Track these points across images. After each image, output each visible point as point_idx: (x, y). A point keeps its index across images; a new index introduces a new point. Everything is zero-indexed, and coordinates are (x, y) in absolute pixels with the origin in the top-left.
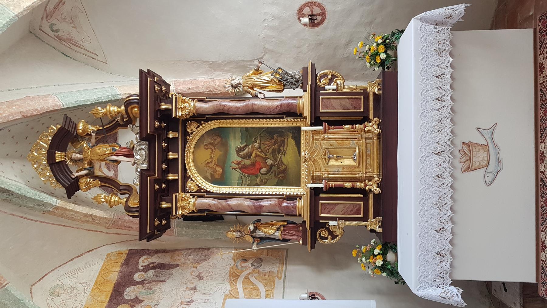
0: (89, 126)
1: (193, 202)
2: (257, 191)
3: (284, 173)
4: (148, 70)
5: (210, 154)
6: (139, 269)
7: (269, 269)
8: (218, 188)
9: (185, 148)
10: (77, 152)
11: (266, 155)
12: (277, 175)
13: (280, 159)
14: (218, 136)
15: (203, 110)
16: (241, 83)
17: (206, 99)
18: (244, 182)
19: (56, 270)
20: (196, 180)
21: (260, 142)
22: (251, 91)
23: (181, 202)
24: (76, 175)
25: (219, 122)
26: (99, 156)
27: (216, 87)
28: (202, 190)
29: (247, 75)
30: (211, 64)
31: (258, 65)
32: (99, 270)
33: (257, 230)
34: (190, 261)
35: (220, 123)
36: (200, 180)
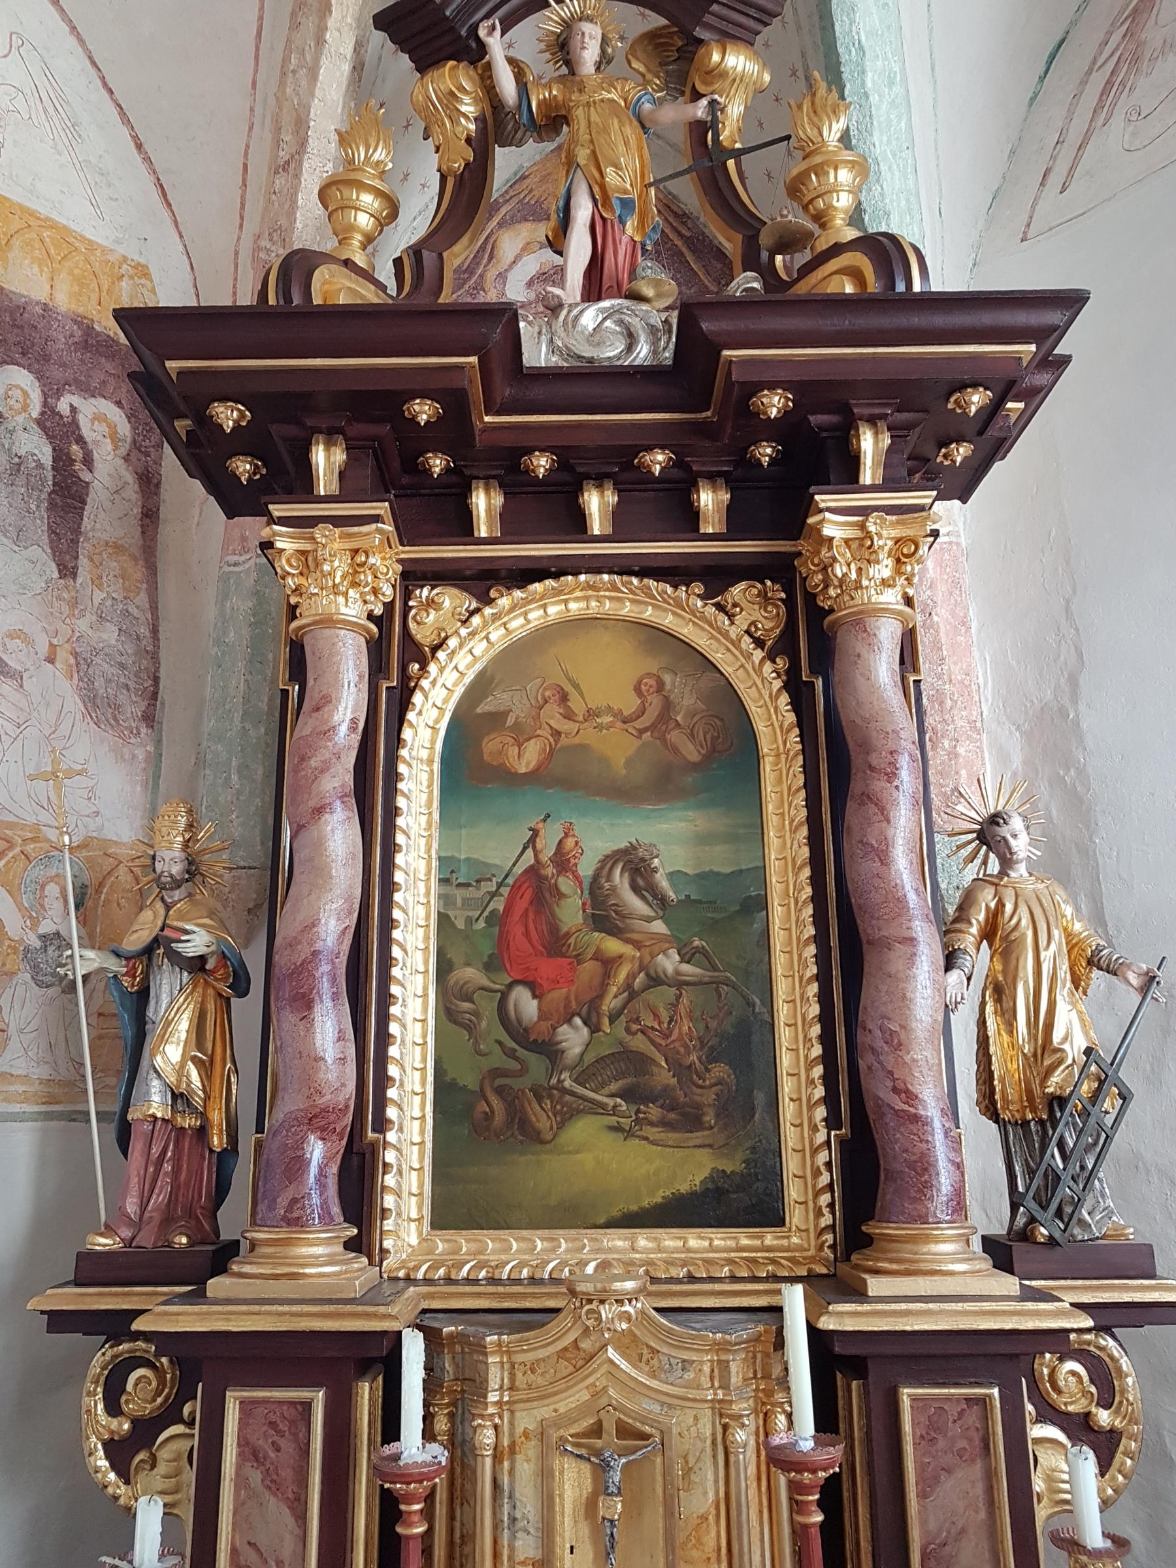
0: (742, 108)
1: (343, 610)
2: (407, 973)
3: (509, 1124)
4: (1065, 361)
5: (609, 709)
6: (59, 394)
7: (21, 1031)
8: (424, 754)
9: (642, 573)
10: (610, 50)
11: (613, 1019)
12: (499, 1082)
13: (592, 1101)
14: (713, 746)
15: (859, 656)
16: (1011, 868)
17: (912, 679)
18: (459, 894)
19: (72, 41)
20: (473, 634)
21: (688, 984)
22: (974, 930)
23: (342, 546)
24: (496, 45)
25: (792, 753)
26: (592, 141)
27: (946, 743)
28: (417, 666)
29: (1063, 906)
30: (1063, 713)
31: (1129, 966)
32: (65, 222)
33: (186, 974)
34: (90, 632)
35: (783, 757)
36: (470, 657)
